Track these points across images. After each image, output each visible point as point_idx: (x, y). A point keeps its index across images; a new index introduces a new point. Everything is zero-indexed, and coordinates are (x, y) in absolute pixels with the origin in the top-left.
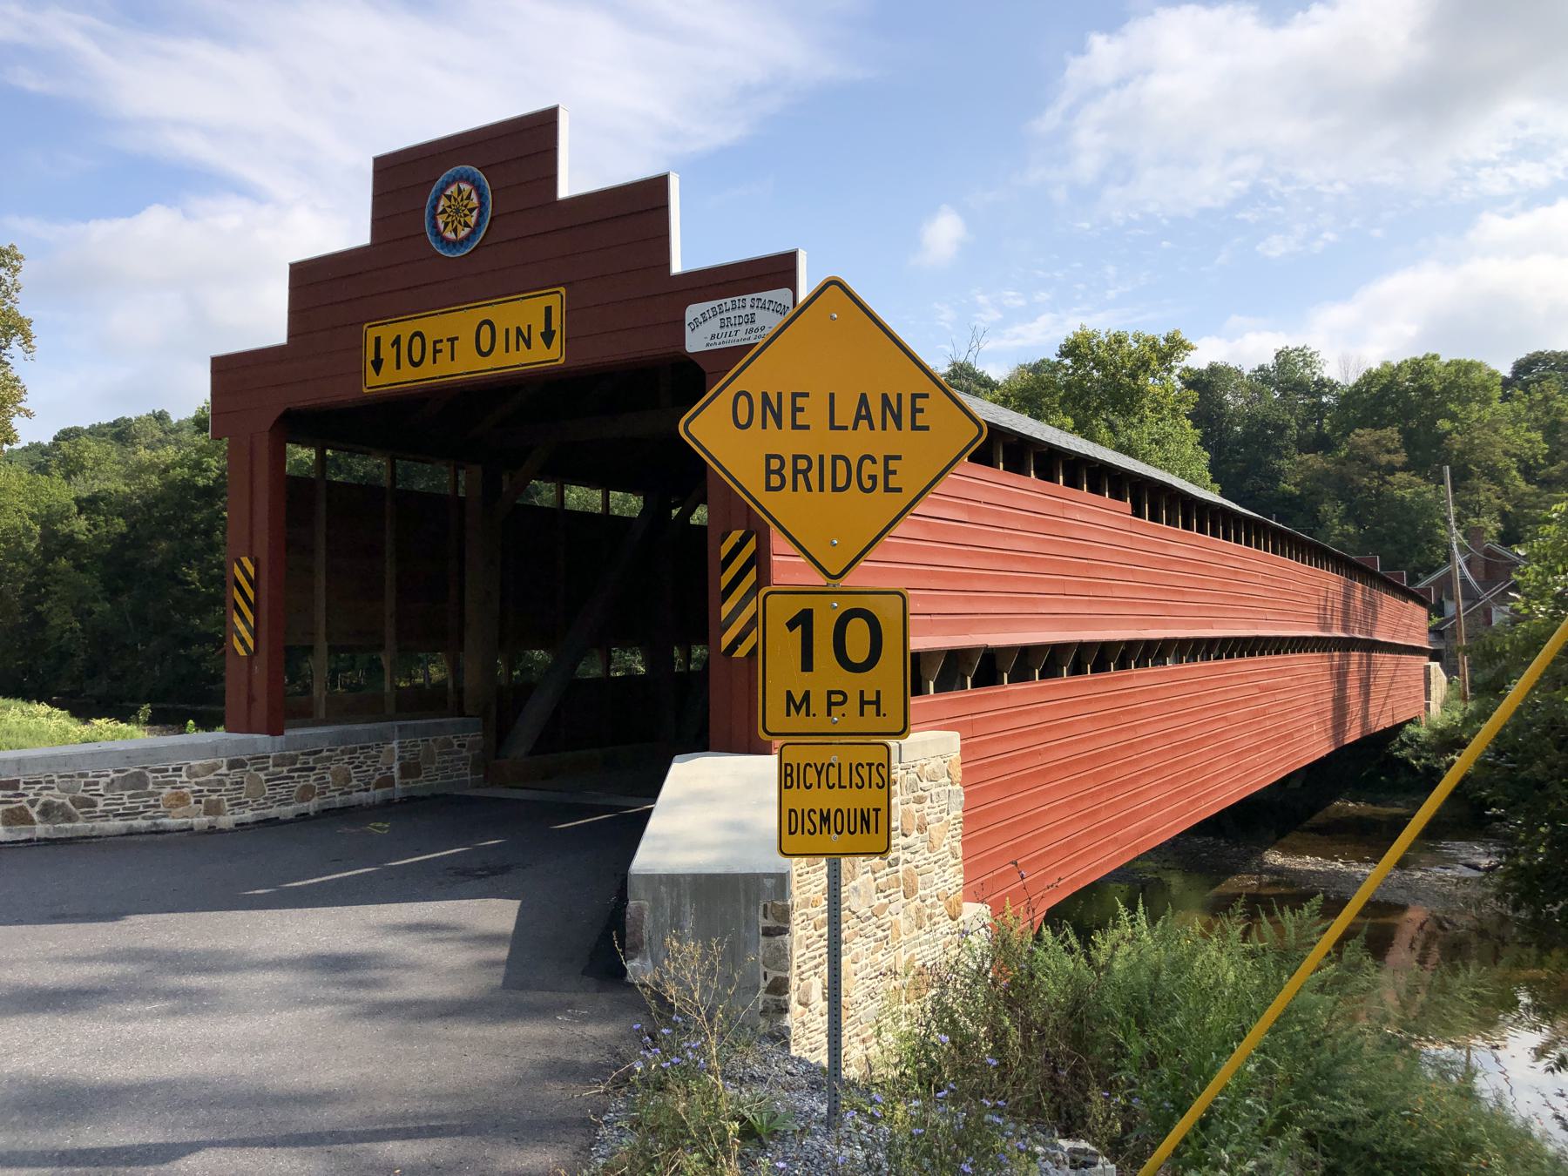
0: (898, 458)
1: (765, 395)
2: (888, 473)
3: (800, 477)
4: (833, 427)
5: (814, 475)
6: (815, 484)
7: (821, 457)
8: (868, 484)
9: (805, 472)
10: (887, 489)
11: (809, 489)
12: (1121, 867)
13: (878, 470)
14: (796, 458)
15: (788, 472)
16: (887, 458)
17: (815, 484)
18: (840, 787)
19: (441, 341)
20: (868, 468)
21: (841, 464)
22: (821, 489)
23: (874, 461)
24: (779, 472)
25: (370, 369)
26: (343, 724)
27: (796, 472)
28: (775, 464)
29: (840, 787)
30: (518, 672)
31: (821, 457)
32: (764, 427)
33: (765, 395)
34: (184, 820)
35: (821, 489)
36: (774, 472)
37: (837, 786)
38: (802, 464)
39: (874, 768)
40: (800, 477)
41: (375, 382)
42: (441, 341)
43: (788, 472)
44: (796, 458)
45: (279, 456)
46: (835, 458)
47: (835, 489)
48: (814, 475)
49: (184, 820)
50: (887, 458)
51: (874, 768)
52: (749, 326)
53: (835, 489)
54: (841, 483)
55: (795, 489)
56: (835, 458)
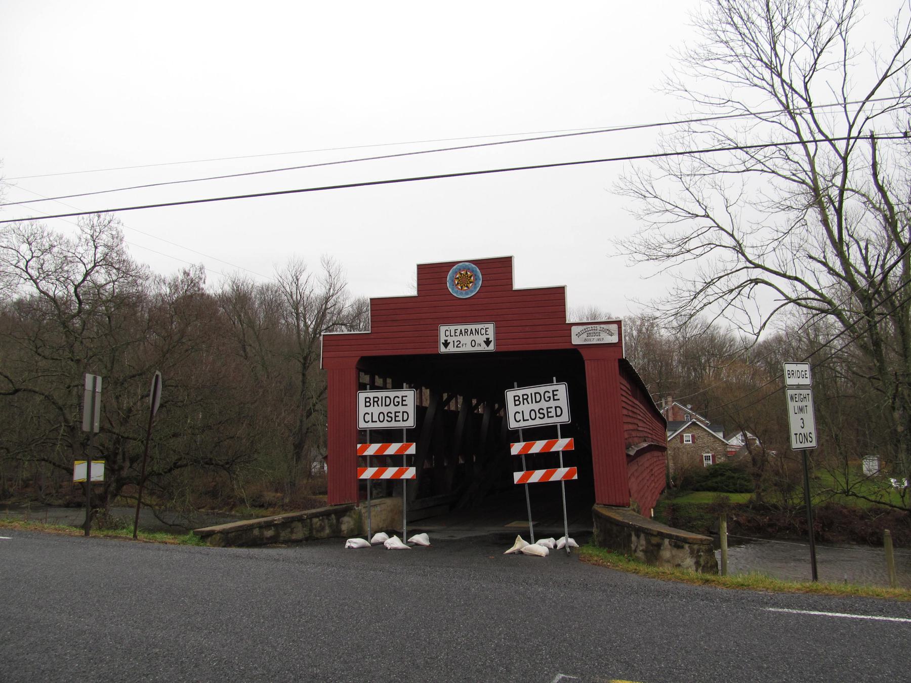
3: (375, 403)
5: (529, 400)
6: (380, 404)
7: (531, 394)
8: (396, 404)
11: (528, 403)
13: (400, 400)
15: (521, 400)
17: (380, 404)
22: (532, 403)
24: (369, 402)
26: (606, 516)
28: (368, 400)
30: (80, 472)
31: (531, 394)
35: (532, 403)
39: (798, 436)
43: (521, 400)
45: (358, 377)
47: (386, 405)
51: (798, 436)
53: (386, 405)
54: (538, 400)
55: (524, 404)
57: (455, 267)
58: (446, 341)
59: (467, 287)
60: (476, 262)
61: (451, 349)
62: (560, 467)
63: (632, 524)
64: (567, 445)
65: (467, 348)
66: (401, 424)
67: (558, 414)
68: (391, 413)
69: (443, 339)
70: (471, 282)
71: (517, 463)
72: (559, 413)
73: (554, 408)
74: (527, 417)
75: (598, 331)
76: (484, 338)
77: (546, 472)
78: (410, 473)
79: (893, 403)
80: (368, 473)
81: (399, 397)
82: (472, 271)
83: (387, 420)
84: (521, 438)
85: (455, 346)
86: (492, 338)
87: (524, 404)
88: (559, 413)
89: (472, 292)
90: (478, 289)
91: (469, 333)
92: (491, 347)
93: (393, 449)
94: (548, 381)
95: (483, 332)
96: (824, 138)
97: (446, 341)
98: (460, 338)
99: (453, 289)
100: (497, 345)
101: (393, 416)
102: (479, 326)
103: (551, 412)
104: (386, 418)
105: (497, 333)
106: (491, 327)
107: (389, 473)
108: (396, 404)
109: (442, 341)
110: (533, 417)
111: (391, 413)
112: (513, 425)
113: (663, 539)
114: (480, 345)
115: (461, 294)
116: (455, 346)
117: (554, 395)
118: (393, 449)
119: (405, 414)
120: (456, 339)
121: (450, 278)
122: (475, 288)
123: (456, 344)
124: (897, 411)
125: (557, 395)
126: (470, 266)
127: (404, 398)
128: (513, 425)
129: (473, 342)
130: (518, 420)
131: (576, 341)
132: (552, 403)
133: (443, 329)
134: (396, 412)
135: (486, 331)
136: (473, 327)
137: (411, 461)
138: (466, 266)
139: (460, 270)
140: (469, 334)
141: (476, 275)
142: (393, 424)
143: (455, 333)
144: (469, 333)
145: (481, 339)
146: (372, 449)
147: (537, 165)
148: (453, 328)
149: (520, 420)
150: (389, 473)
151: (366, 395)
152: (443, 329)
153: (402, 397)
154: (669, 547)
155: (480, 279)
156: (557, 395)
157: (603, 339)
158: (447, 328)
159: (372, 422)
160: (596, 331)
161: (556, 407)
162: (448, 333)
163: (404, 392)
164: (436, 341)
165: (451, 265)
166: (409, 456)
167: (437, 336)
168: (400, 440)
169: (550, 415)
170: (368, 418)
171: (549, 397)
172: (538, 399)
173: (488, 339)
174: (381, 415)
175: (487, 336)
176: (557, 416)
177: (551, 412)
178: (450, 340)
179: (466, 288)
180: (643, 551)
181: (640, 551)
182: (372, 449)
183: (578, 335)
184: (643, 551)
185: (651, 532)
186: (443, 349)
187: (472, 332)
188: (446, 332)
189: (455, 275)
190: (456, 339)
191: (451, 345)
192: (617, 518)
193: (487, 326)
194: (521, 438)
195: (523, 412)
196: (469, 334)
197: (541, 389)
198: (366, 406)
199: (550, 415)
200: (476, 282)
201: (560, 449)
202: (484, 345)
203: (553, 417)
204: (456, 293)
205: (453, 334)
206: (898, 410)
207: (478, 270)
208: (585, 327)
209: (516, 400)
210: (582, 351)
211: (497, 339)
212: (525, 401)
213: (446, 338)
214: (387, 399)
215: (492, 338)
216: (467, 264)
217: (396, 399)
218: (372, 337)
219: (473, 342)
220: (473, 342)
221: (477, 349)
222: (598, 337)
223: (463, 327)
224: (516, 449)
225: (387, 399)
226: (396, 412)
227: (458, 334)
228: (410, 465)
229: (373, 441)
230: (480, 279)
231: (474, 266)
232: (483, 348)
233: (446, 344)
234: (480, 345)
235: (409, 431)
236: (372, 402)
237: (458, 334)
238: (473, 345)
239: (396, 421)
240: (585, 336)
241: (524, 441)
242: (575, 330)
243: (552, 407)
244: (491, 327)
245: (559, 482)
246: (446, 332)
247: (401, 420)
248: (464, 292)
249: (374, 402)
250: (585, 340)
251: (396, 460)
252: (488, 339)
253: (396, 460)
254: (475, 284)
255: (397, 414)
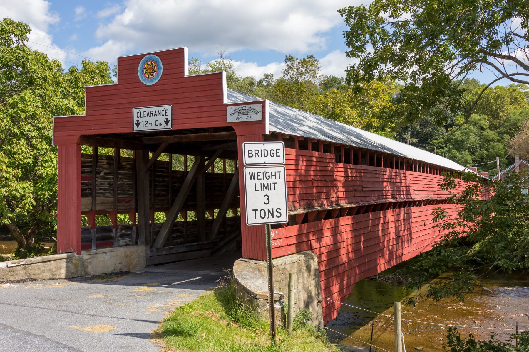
1: (268, 210)
3: (256, 154)
4: (256, 190)
9: (257, 153)
13: (275, 152)
14: (255, 150)
15: (253, 153)
16: (277, 150)
19: (260, 173)
20: (272, 152)
21: (266, 152)
25: (135, 126)
27: (255, 153)
32: (273, 209)
33: (268, 210)
38: (257, 152)
40: (256, 154)
41: (135, 129)
42: (260, 173)
43: (253, 153)
44: (255, 150)
45: (79, 149)
46: (264, 150)
47: (265, 156)
48: (259, 154)
50: (277, 150)
52: (247, 116)
53: (265, 156)
54: (266, 155)
56: (264, 150)
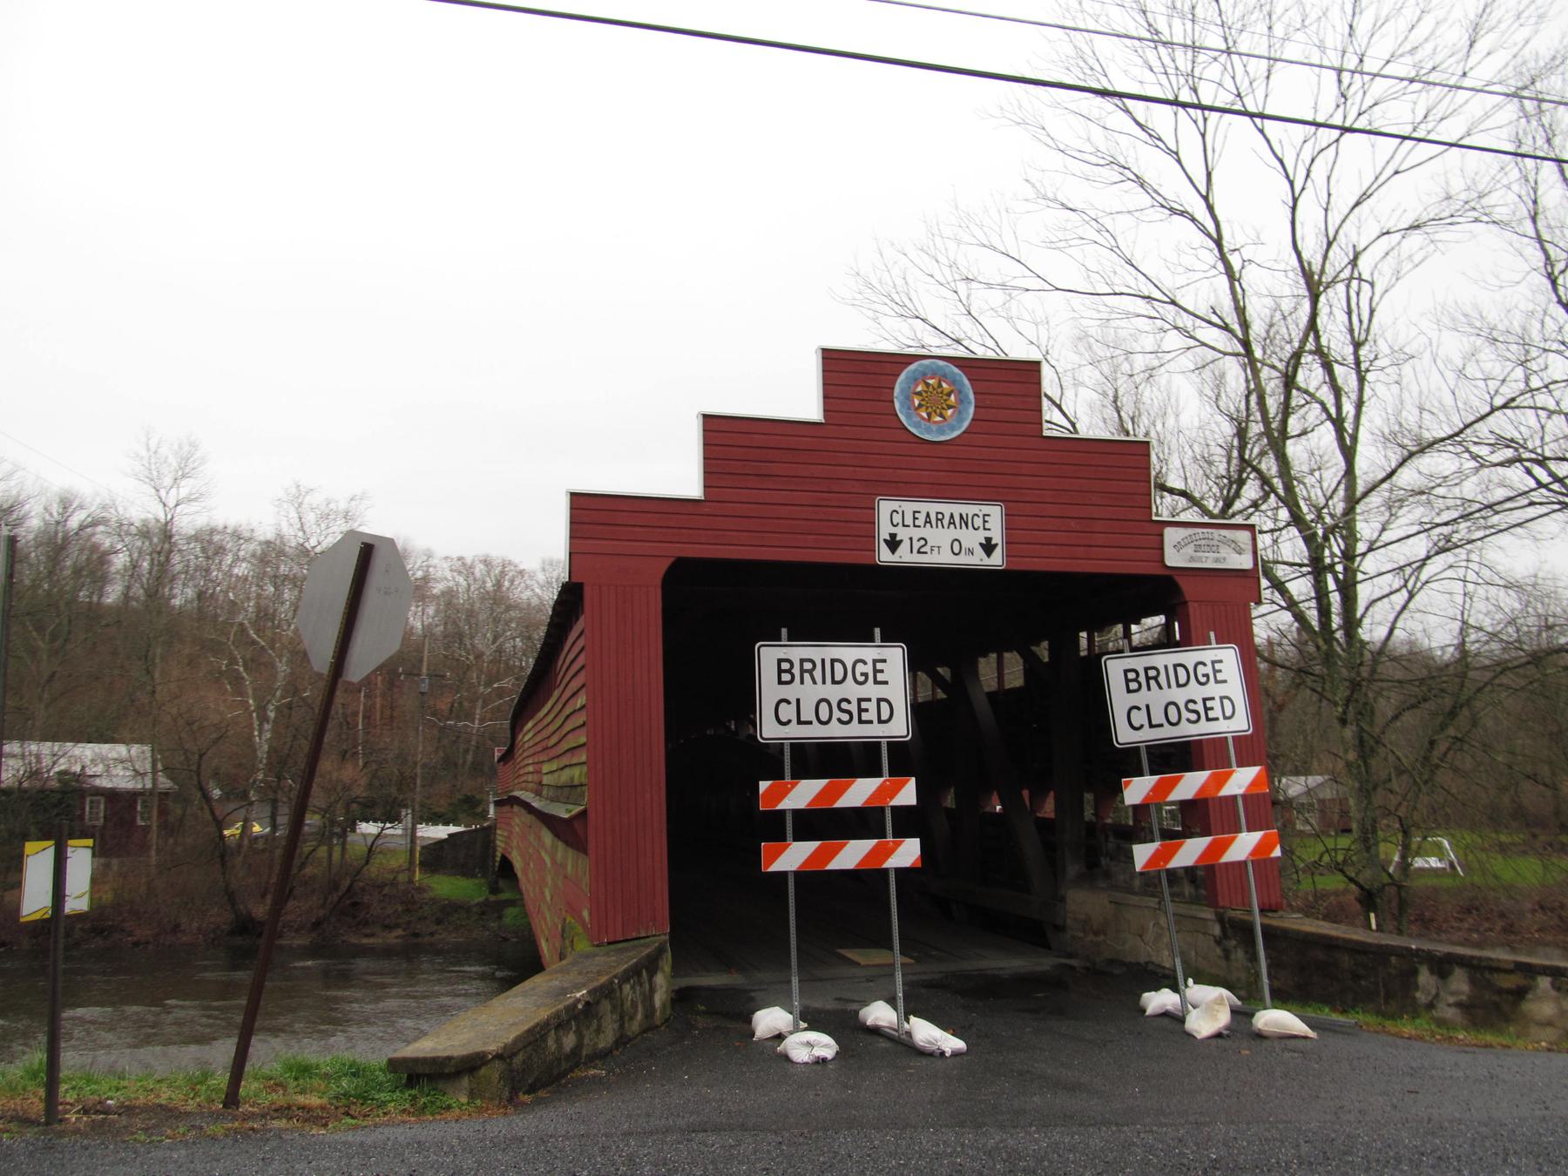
0: (1221, 661)
2: (1216, 671)
5: (818, 674)
7: (823, 661)
9: (811, 672)
10: (1217, 682)
11: (815, 682)
12: (1189, 619)
13: (869, 669)
18: (904, 526)
22: (824, 682)
23: (1205, 664)
29: (904, 526)
31: (823, 661)
34: (372, 1138)
35: (824, 682)
36: (785, 671)
37: (901, 524)
38: (808, 666)
46: (1175, 666)
47: (1179, 685)
49: (372, 1138)
53: (1179, 685)
54: (838, 677)
55: (1149, 689)
57: (913, 367)
58: (893, 536)
59: (941, 415)
60: (972, 366)
61: (904, 556)
62: (1241, 832)
63: (1418, 950)
64: (1254, 783)
65: (943, 557)
66: (875, 731)
67: (1228, 713)
68: (849, 702)
69: (885, 531)
70: (950, 407)
71: (906, 822)
72: (885, 716)
73: (874, 702)
74: (1158, 717)
75: (1215, 543)
76: (981, 536)
77: (818, 850)
78: (908, 853)
79: (1344, 713)
80: (793, 856)
81: (865, 663)
82: (952, 383)
83: (839, 720)
84: (1146, 766)
85: (915, 550)
86: (997, 538)
87: (1149, 689)
88: (885, 716)
89: (953, 429)
90: (966, 424)
91: (946, 522)
92: (997, 560)
93: (859, 792)
94: (864, 637)
95: (978, 522)
96: (1204, 193)
97: (893, 536)
98: (926, 532)
99: (908, 417)
100: (1009, 555)
101: (853, 708)
102: (969, 509)
103: (867, 710)
104: (837, 714)
105: (1010, 527)
106: (995, 513)
107: (852, 854)
108: (1203, 680)
109: (884, 535)
110: (824, 717)
111: (849, 702)
112: (1124, 735)
113: (1533, 979)
114: (971, 552)
115: (929, 431)
116: (915, 550)
117: (876, 671)
118: (859, 792)
119: (884, 705)
120: (916, 533)
121: (902, 390)
122: (961, 421)
123: (916, 545)
124: (1349, 726)
125: (882, 671)
126: (947, 370)
127: (879, 666)
128: (1124, 735)
129: (956, 545)
130: (1136, 724)
131: (1173, 559)
132: (871, 690)
133: (885, 507)
134: (860, 701)
135: (985, 521)
136: (957, 509)
137: (906, 822)
138: (939, 367)
139: (924, 374)
140: (946, 526)
141: (960, 392)
142: (855, 731)
143: (915, 518)
144: (946, 522)
145: (972, 539)
146: (803, 794)
147: (1194, 191)
148: (908, 507)
149: (789, 721)
150: (852, 854)
151: (782, 653)
152: (885, 507)
153: (875, 662)
154: (1553, 993)
155: (969, 403)
156: (882, 671)
157: (1224, 559)
158: (894, 505)
159: (800, 722)
160: (1211, 543)
161: (879, 700)
162: (897, 518)
163: (784, 649)
164: (870, 536)
165: (901, 361)
166: (898, 811)
167: (871, 523)
168: (875, 772)
169: (865, 716)
170: (787, 712)
171: (865, 675)
172: (1182, 679)
173: (988, 540)
174: (824, 707)
175: (988, 534)
176: (880, 721)
177: (867, 710)
178: (902, 534)
179: (938, 419)
180: (1458, 1005)
181: (1449, 1005)
182: (803, 794)
183: (1178, 547)
184: (1458, 1005)
185: (1494, 965)
186: (885, 556)
187: (952, 522)
188: (890, 513)
189: (912, 386)
190: (916, 533)
191: (904, 548)
192: (1355, 937)
193: (986, 509)
194: (1146, 766)
195: (798, 701)
196: (946, 526)
197: (848, 653)
198: (1129, 691)
199: (865, 716)
200: (961, 407)
201: (1240, 791)
202: (980, 552)
203: (871, 722)
204: (917, 426)
205: (909, 521)
206: (1351, 724)
207: (966, 382)
208: (1190, 531)
209: (784, 672)
210: (1182, 582)
211: (1009, 542)
212: (807, 676)
213: (893, 530)
214: (1179, 669)
215: (997, 538)
216: (941, 363)
217: (860, 668)
218: (707, 510)
219: (956, 543)
220: (956, 545)
221: (964, 560)
222: (1216, 555)
223: (933, 508)
224: (1137, 790)
225: (1179, 669)
226: (860, 701)
227: (920, 522)
228: (902, 832)
229: (802, 772)
230: (969, 403)
231: (956, 370)
232: (978, 559)
233: (893, 544)
234: (971, 552)
235: (896, 747)
236: (796, 670)
237: (920, 522)
238: (956, 551)
239: (861, 721)
240: (1190, 550)
241: (1152, 773)
242: (1171, 536)
243: (869, 700)
244: (995, 513)
245: (1241, 865)
246: (890, 513)
247: (875, 721)
248: (934, 428)
249: (802, 671)
250: (1192, 559)
251: (862, 822)
252: (988, 540)
253: (862, 822)
254: (960, 413)
255: (864, 705)
